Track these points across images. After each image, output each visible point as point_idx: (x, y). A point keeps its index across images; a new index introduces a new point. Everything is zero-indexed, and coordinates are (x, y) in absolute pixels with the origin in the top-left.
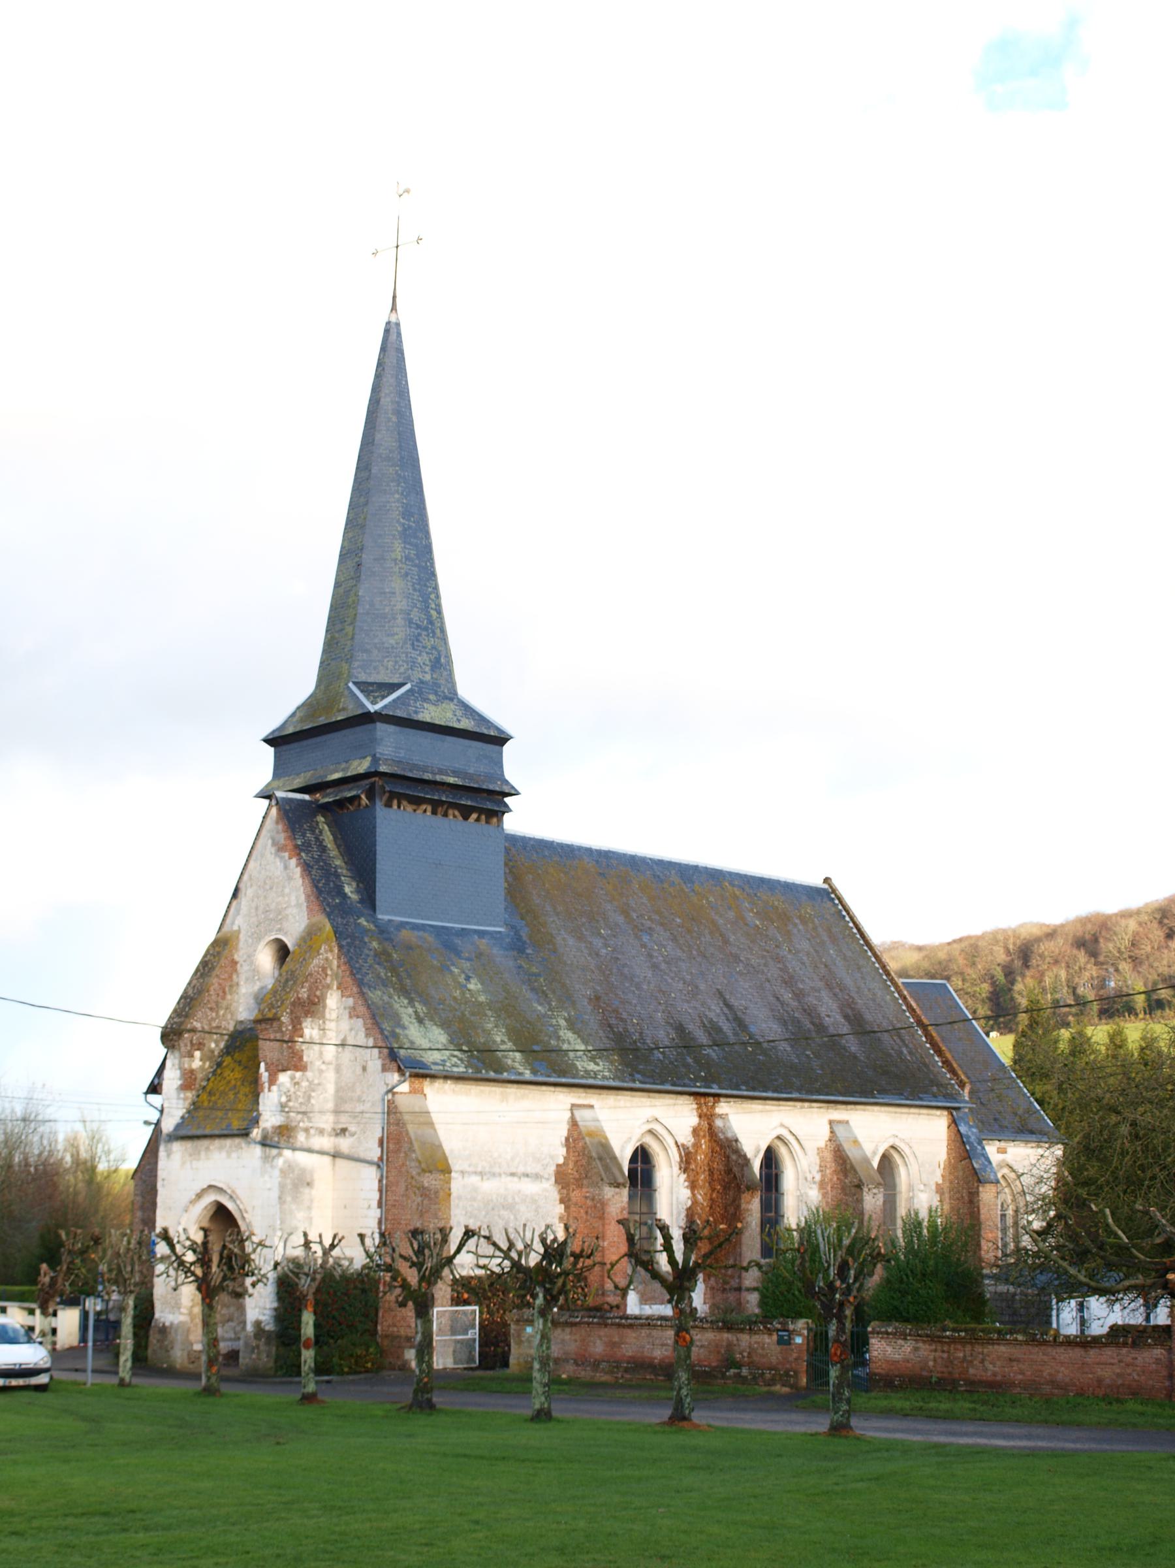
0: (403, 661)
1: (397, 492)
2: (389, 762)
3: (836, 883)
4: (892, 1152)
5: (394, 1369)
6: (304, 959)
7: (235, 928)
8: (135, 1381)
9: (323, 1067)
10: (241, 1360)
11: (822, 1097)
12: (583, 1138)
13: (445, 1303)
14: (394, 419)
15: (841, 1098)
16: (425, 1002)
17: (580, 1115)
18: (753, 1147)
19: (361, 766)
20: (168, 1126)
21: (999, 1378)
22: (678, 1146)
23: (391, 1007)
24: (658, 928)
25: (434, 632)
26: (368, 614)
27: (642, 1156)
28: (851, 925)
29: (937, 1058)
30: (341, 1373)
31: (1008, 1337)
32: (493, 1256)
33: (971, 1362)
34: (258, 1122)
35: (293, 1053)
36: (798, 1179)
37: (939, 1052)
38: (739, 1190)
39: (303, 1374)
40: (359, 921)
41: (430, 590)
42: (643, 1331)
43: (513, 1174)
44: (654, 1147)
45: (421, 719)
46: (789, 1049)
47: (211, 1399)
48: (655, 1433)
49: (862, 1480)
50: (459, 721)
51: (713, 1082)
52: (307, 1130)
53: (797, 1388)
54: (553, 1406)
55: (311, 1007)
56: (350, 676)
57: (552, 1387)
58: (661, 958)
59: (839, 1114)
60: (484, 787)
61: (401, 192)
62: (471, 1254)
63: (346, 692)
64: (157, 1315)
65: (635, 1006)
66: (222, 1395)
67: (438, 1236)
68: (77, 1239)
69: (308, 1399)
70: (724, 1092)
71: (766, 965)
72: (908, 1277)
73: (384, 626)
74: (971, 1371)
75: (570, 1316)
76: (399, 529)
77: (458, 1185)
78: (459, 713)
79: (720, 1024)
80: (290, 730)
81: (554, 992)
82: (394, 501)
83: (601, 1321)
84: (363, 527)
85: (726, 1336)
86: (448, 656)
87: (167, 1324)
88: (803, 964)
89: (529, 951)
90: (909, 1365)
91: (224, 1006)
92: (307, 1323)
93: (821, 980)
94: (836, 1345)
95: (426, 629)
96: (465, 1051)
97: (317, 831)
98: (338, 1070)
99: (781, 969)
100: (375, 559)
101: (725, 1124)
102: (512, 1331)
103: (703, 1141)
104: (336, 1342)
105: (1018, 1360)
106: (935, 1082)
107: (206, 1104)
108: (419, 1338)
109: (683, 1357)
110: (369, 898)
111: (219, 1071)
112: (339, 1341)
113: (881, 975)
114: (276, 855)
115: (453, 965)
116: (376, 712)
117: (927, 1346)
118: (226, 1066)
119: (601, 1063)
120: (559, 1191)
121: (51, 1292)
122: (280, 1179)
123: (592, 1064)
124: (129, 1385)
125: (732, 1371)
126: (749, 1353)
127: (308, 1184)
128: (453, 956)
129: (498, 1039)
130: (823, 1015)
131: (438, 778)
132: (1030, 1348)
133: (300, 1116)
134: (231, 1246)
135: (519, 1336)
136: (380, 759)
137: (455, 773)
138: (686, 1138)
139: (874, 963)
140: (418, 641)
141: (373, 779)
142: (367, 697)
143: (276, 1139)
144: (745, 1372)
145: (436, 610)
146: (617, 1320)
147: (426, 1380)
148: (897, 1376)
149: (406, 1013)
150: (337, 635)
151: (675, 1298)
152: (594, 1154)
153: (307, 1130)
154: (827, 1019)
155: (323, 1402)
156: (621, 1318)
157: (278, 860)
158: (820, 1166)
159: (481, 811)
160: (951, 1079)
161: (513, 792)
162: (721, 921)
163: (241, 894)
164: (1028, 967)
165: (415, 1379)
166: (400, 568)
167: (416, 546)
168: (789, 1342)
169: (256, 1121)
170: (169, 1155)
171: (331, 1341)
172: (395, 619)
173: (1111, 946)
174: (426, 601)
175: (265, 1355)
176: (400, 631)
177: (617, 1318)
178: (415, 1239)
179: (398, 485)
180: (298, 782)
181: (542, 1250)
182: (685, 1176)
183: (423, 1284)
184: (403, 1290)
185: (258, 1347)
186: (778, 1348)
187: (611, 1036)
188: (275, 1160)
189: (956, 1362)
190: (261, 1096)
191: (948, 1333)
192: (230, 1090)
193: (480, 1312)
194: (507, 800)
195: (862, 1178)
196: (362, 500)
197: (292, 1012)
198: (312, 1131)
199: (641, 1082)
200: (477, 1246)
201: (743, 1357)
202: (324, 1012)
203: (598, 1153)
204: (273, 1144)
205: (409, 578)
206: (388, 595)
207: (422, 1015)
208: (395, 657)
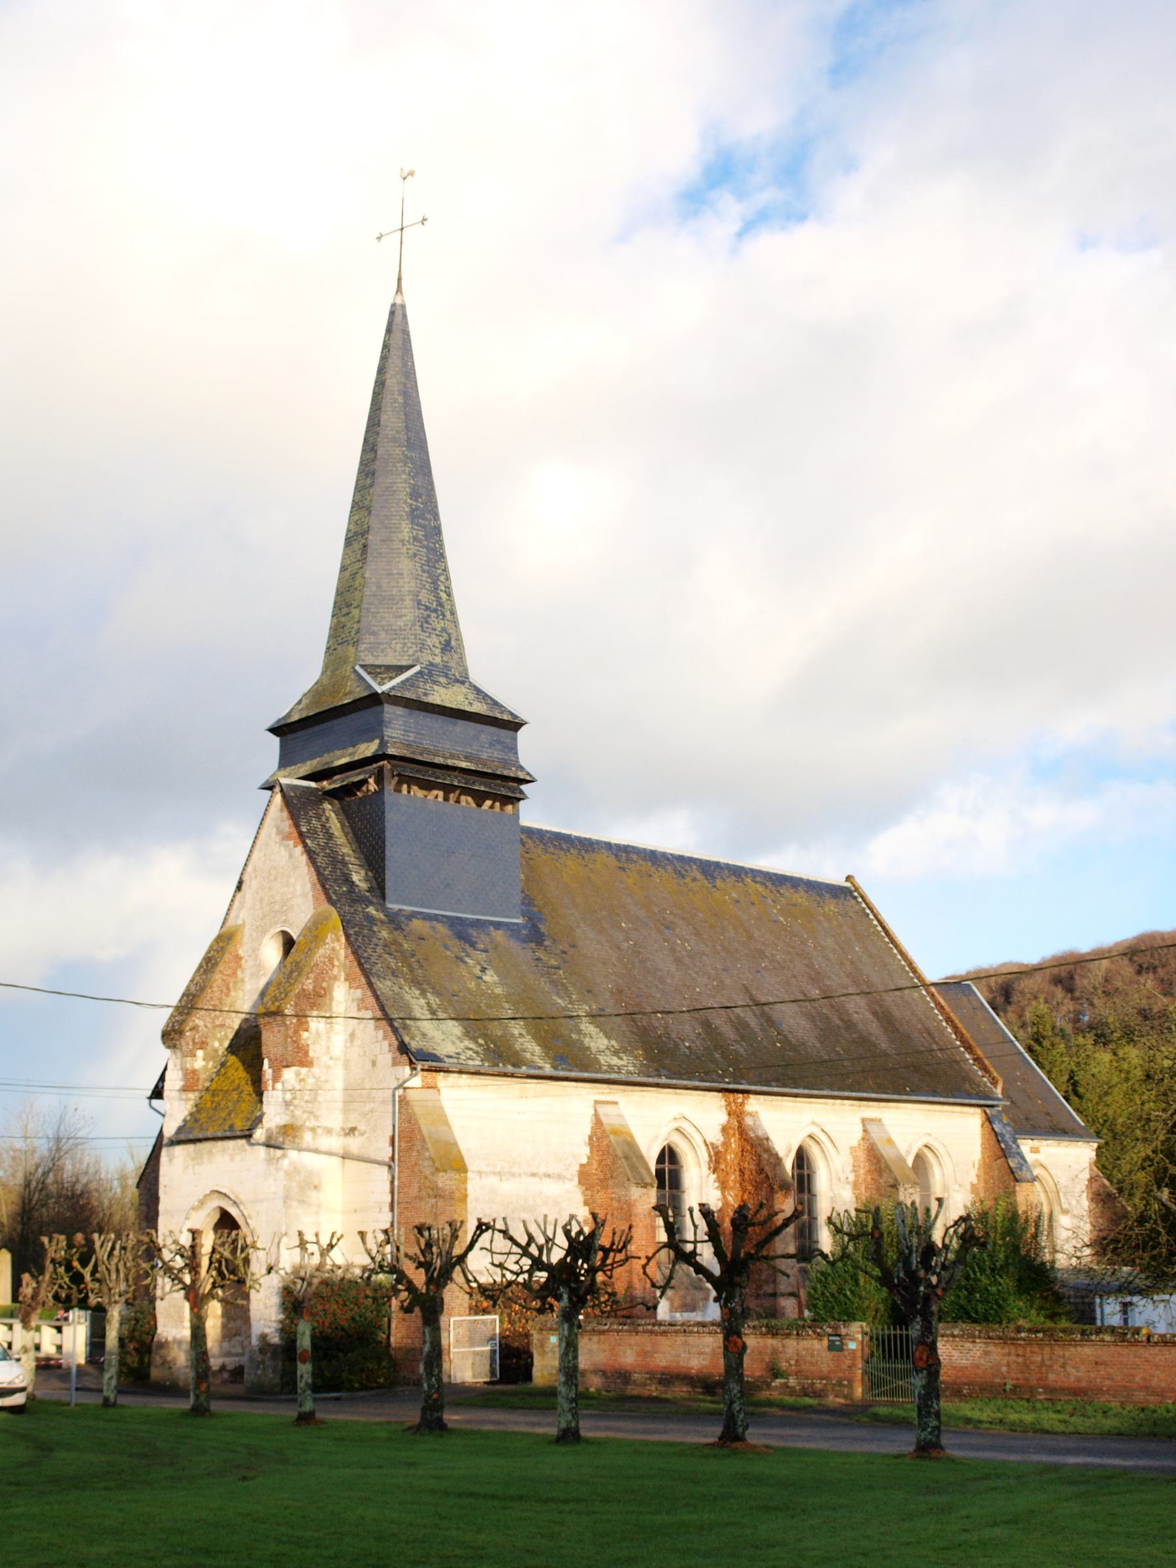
0: (412, 643)
1: (404, 472)
2: (398, 745)
3: (860, 881)
4: (926, 1151)
5: (409, 1384)
6: (310, 949)
7: (240, 922)
8: (123, 1400)
9: (331, 1063)
10: (246, 1376)
11: (854, 1094)
12: (608, 1136)
13: (462, 1313)
14: (401, 400)
15: (874, 1095)
16: (438, 994)
17: (602, 1110)
18: (785, 1148)
19: (368, 749)
20: (169, 1132)
21: (1083, 1384)
22: (707, 1145)
23: (402, 998)
24: (680, 922)
25: (444, 615)
26: (375, 595)
27: (669, 1156)
28: (875, 922)
29: (967, 1056)
30: (352, 1389)
31: (1093, 1337)
32: (509, 1253)
33: (1051, 1366)
34: (261, 1121)
35: (298, 1047)
36: (831, 1180)
37: (969, 1048)
38: (772, 1190)
39: (299, 1391)
40: (367, 910)
41: (439, 571)
42: (678, 1339)
43: (533, 1175)
44: (682, 1148)
45: (431, 702)
46: (818, 1045)
47: (199, 1421)
48: (705, 1457)
49: (995, 1524)
50: (471, 704)
51: (742, 1078)
52: (313, 1130)
53: (851, 1399)
54: (581, 1424)
55: (317, 998)
56: (357, 658)
57: (579, 1402)
58: (684, 953)
59: (872, 1110)
60: (498, 773)
61: (405, 174)
62: (484, 1251)
63: (353, 676)
64: (159, 1330)
65: (659, 1001)
66: (212, 1415)
67: (447, 1230)
68: (60, 1246)
69: (305, 1418)
70: (753, 1088)
71: (791, 961)
72: (974, 1273)
73: (392, 608)
74: (1051, 1376)
75: (598, 1324)
76: (407, 509)
77: (474, 1186)
78: (471, 696)
79: (747, 1019)
80: (296, 717)
81: (574, 985)
82: (400, 482)
83: (631, 1328)
84: (369, 510)
85: (771, 1342)
86: (459, 639)
87: (170, 1339)
88: (828, 960)
89: (546, 943)
90: (980, 1372)
91: (228, 1004)
92: (304, 1333)
93: (847, 976)
94: (921, 1348)
95: (435, 611)
96: (481, 1045)
97: (323, 818)
98: (346, 1066)
99: (807, 966)
100: (381, 541)
101: (755, 1121)
102: (535, 1341)
103: (733, 1140)
104: (345, 1356)
105: (1105, 1364)
106: (967, 1078)
107: (209, 1105)
108: (427, 1348)
109: (734, 1365)
110: (379, 888)
111: (223, 1071)
112: (349, 1355)
113: (908, 972)
114: (281, 844)
115: (468, 956)
116: (383, 693)
117: (1000, 1350)
118: (230, 1066)
119: (625, 1058)
120: (583, 1193)
121: (34, 1304)
122: (285, 1182)
123: (615, 1058)
124: (114, 1405)
125: (778, 1382)
126: (797, 1361)
127: (316, 1187)
128: (467, 947)
129: (516, 1032)
130: (851, 1011)
131: (450, 762)
132: (1119, 1349)
133: (306, 1116)
134: (221, 1249)
135: (542, 1346)
136: (387, 742)
137: (467, 758)
138: (716, 1137)
139: (900, 961)
140: (427, 622)
141: (381, 763)
142: (375, 678)
143: (281, 1139)
144: (792, 1381)
145: (445, 592)
146: (649, 1327)
147: (435, 1396)
148: (965, 1384)
149: (418, 1004)
150: (343, 619)
151: (724, 1296)
152: (619, 1153)
153: (313, 1130)
154: (855, 1015)
155: (323, 1422)
156: (654, 1325)
157: (282, 849)
158: (854, 1166)
159: (495, 797)
160: (983, 1077)
161: (528, 778)
162: (745, 917)
163: (244, 887)
164: (1009, 1003)
165: (423, 1396)
166: (407, 549)
167: (424, 526)
168: (840, 1349)
169: (259, 1120)
170: (171, 1160)
171: (341, 1355)
172: (403, 600)
173: (1085, 982)
174: (435, 583)
175: (271, 1371)
176: (409, 614)
177: (649, 1324)
178: (422, 1236)
179: (405, 465)
180: (307, 768)
181: (566, 1244)
182: (715, 1176)
183: (431, 1287)
184: (409, 1293)
185: (263, 1362)
186: (830, 1355)
187: (635, 1030)
188: (280, 1162)
189: (1032, 1367)
190: (265, 1093)
191: (1023, 1335)
192: (234, 1090)
193: (500, 1321)
194: (524, 787)
195: (898, 1178)
196: (369, 481)
197: (296, 1004)
198: (319, 1131)
199: (668, 1077)
200: (492, 1241)
201: (790, 1365)
202: (331, 1003)
203: (623, 1152)
204: (278, 1144)
205: (417, 559)
206: (396, 577)
207: (435, 1006)
208: (404, 639)
